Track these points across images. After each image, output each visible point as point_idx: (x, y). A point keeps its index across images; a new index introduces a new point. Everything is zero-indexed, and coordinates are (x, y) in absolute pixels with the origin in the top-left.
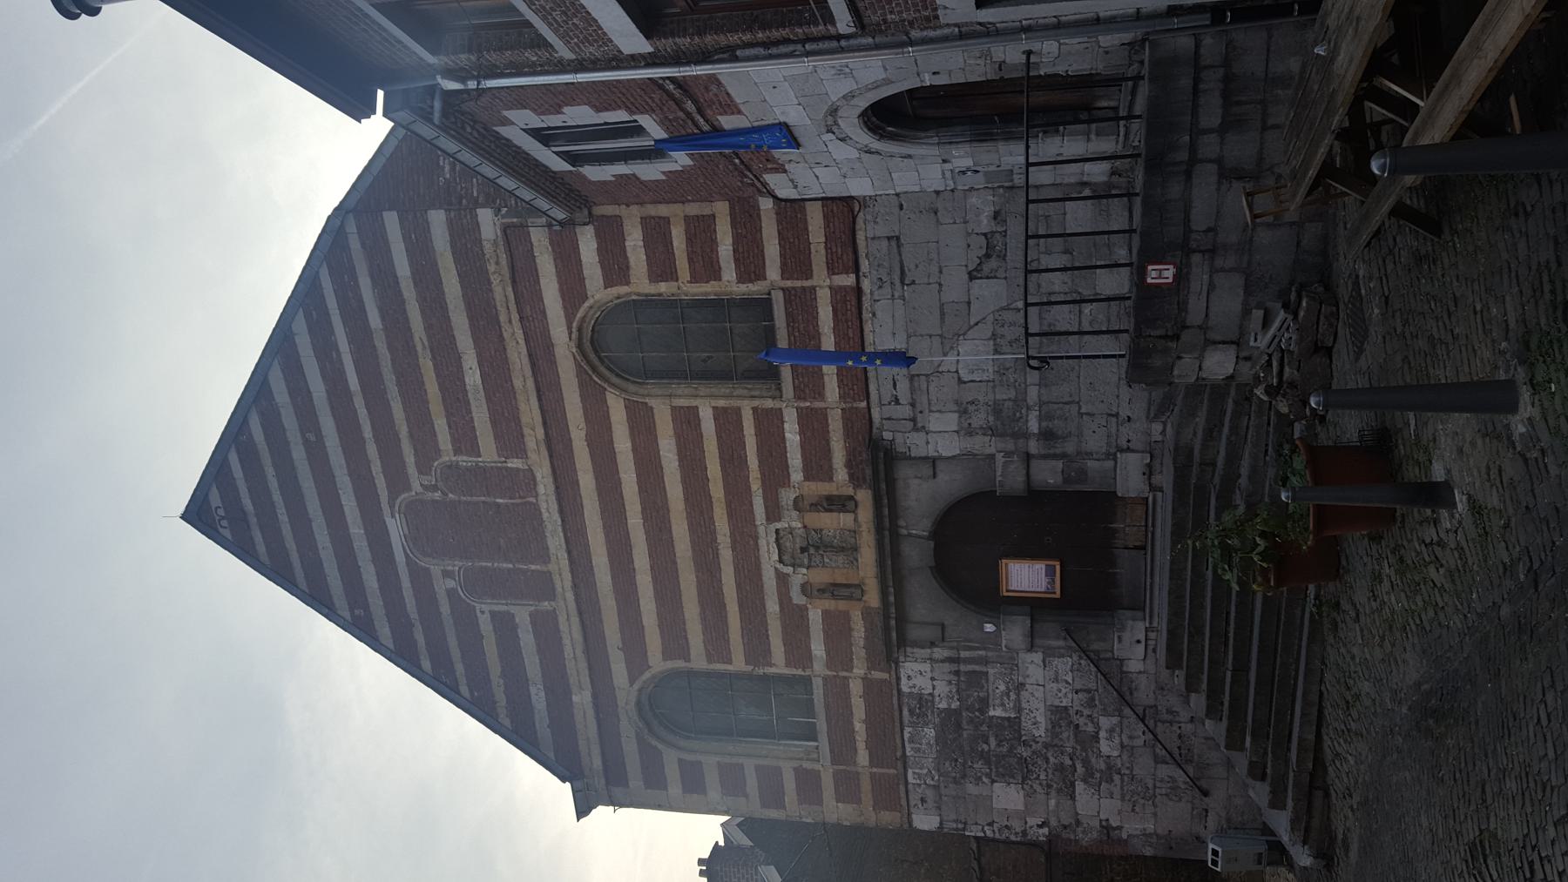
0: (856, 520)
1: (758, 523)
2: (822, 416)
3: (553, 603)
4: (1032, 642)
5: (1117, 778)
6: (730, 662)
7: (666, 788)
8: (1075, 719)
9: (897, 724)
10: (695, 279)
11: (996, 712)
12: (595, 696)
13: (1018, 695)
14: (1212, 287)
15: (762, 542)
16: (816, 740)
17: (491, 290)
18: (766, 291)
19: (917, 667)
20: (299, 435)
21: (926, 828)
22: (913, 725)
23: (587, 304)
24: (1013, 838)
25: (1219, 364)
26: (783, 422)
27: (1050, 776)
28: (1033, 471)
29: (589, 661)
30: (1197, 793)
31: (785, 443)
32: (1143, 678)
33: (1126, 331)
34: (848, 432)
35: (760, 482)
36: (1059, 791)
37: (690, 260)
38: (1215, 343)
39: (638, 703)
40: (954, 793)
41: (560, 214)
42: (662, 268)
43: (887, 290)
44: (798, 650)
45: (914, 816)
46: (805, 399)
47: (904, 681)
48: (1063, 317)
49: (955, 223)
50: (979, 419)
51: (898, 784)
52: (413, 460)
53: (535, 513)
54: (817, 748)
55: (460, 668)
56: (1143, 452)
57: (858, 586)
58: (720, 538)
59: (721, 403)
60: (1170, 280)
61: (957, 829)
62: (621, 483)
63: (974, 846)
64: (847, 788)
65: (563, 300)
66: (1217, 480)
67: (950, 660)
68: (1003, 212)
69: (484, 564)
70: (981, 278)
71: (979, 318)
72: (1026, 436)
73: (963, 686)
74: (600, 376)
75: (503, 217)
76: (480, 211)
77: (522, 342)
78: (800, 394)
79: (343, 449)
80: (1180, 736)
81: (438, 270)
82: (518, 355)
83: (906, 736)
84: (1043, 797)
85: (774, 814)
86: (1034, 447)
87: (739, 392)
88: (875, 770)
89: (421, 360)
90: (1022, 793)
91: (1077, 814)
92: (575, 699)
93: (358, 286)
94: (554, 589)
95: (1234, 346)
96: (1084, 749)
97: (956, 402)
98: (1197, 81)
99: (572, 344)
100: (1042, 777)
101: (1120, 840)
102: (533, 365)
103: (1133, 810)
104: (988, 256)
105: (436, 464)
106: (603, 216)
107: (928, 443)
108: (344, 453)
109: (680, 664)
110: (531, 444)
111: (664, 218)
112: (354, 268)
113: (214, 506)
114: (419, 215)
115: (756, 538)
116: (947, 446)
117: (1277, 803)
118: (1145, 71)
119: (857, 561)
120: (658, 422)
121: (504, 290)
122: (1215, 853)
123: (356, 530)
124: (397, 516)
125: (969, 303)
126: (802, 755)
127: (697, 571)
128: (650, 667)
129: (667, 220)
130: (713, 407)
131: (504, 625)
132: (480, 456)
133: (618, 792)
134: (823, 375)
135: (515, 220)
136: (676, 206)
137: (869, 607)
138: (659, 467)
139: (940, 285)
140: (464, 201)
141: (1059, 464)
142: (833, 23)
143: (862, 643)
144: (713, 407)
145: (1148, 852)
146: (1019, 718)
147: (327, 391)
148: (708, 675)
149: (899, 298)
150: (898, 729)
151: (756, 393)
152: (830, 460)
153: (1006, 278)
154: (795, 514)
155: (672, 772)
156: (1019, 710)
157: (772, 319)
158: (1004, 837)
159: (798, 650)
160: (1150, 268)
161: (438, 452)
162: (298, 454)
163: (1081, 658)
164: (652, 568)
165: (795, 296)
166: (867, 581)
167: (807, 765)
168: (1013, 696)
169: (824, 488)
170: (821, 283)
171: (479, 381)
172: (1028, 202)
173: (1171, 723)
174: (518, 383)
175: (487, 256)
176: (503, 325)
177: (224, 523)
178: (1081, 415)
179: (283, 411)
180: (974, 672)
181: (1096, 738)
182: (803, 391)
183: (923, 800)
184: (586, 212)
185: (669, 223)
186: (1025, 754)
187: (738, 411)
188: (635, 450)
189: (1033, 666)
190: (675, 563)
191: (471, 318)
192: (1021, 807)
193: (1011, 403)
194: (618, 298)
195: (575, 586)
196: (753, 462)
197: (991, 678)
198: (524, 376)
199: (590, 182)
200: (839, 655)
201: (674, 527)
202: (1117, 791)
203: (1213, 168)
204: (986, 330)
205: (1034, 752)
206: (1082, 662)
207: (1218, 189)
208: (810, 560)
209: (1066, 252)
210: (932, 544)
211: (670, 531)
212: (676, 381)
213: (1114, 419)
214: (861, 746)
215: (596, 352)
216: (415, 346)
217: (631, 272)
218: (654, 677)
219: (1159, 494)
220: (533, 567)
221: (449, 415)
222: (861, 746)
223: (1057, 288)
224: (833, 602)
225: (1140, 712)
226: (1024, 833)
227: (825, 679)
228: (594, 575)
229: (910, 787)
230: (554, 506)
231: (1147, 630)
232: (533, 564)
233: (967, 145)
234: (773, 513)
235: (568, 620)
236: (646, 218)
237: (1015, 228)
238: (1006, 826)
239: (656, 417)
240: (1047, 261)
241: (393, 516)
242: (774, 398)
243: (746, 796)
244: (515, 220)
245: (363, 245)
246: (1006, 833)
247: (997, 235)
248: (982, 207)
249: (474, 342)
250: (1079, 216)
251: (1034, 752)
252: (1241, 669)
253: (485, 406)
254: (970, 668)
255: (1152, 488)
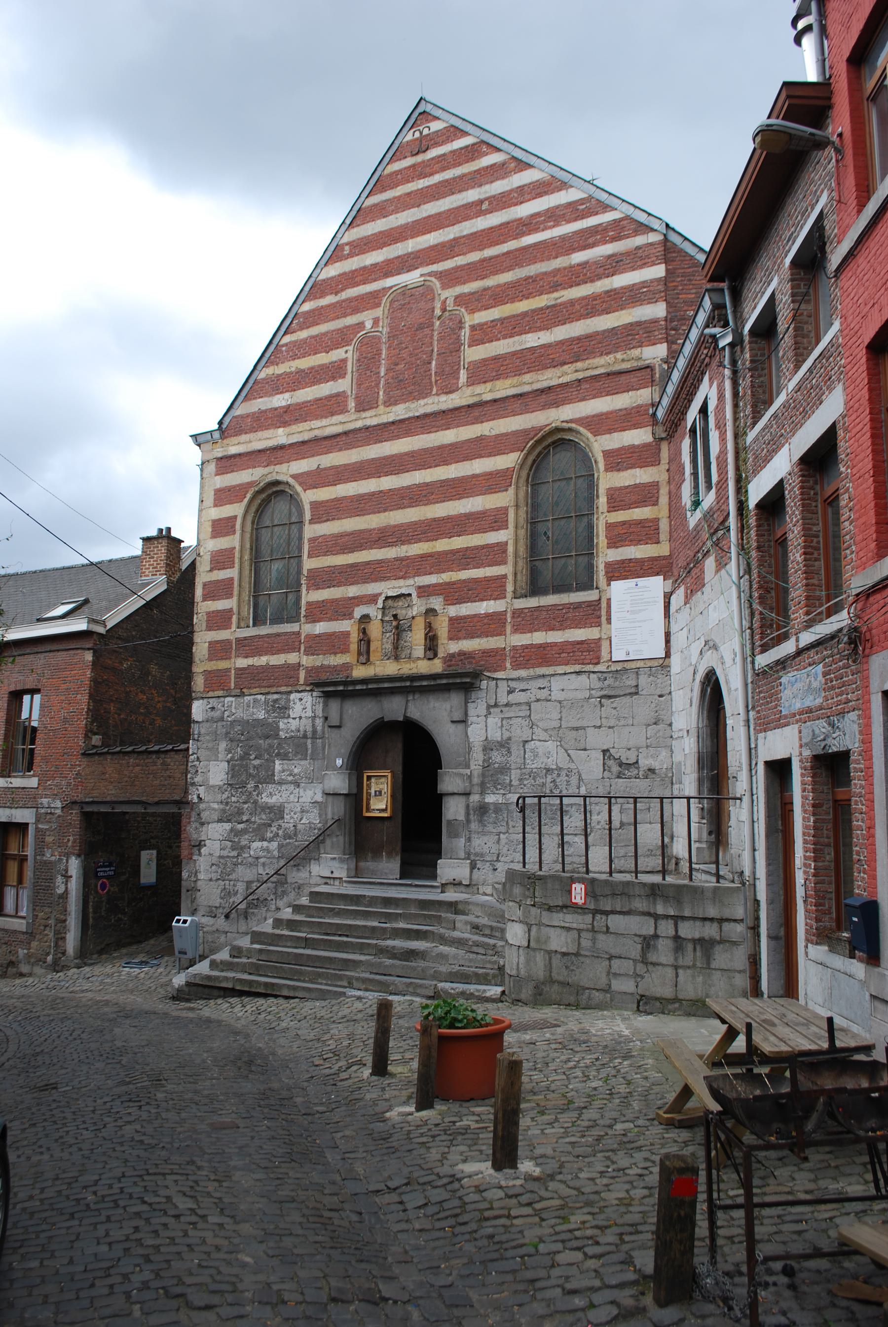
0: (419, 658)
1: (416, 579)
2: (501, 633)
3: (353, 410)
4: (329, 794)
5: (235, 853)
6: (310, 556)
7: (215, 505)
8: (275, 824)
9: (267, 690)
10: (609, 526)
11: (278, 765)
12: (282, 447)
13: (291, 783)
14: (568, 929)
15: (401, 582)
16: (254, 625)
17: (602, 355)
18: (600, 586)
19: (309, 705)
20: (487, 195)
21: (194, 711)
22: (266, 702)
23: (590, 435)
24: (189, 776)
25: (516, 933)
26: (495, 599)
27: (234, 805)
28: (456, 798)
29: (309, 441)
30: (227, 910)
31: (479, 601)
32: (307, 875)
33: (541, 869)
34: (488, 653)
35: (448, 580)
36: (224, 811)
37: (624, 523)
38: (529, 930)
39: (277, 483)
40: (218, 732)
41: (660, 413)
42: (618, 500)
43: (599, 685)
44: (319, 612)
45: (201, 701)
46: (513, 617)
47: (299, 695)
48: (574, 821)
49: (647, 738)
50: (497, 757)
51: (223, 690)
52: (466, 291)
53: (424, 393)
54: (248, 627)
55: (303, 334)
56: (471, 879)
57: (368, 660)
58: (404, 548)
59: (511, 549)
60: (574, 901)
61: (194, 734)
62: (447, 465)
63: (183, 747)
64: (219, 650)
65: (593, 416)
66: (442, 931)
67: (314, 731)
68: (654, 776)
69: (384, 352)
70: (604, 759)
71: (573, 757)
72: (482, 793)
73: (296, 741)
74: (533, 447)
75: (660, 365)
76: (664, 346)
77: (561, 381)
78: (517, 613)
79: (476, 233)
80: (266, 899)
81: (617, 311)
82: (549, 378)
83: (259, 697)
84: (219, 799)
85: (199, 592)
86: (475, 798)
87: (521, 563)
88: (233, 672)
89: (546, 296)
90: (221, 783)
91: (209, 823)
92: (281, 430)
93: (605, 243)
94: (364, 410)
95: (526, 945)
96: (254, 830)
97: (509, 739)
98: (712, 920)
99: (558, 424)
100: (233, 799)
101: (192, 854)
102: (542, 391)
103: (213, 864)
104: (621, 764)
105: (463, 310)
106: (660, 450)
107: (478, 716)
108: (472, 234)
109: (308, 516)
110: (479, 389)
111: (657, 501)
112: (620, 240)
113: (430, 125)
114: (663, 294)
115: (404, 577)
116: (476, 733)
117: (214, 965)
118: (725, 884)
119: (388, 659)
120: (495, 496)
121: (603, 366)
122: (185, 922)
123: (411, 245)
124: (422, 279)
125: (585, 750)
126: (242, 614)
127: (379, 529)
128: (305, 490)
129: (655, 503)
130: (507, 542)
131: (335, 371)
132: (469, 346)
133: (212, 468)
134: (531, 632)
135: (657, 375)
136: (667, 511)
137: (352, 670)
138: (459, 496)
139: (600, 727)
140: (673, 332)
141: (461, 817)
142: (762, 652)
143: (325, 663)
144: (507, 542)
145: (185, 875)
146: (274, 783)
147: (521, 219)
148: (300, 538)
149: (591, 694)
150: (264, 690)
151: (519, 577)
152: (465, 638)
153: (603, 778)
154: (423, 609)
155: (228, 511)
156: (281, 783)
157: (578, 590)
158: (189, 769)
159: (319, 612)
160: (583, 886)
161: (472, 312)
162: (472, 195)
163: (320, 829)
164: (381, 492)
165: (594, 610)
166: (372, 667)
167: (234, 619)
168: (290, 778)
169: (442, 629)
170: (604, 631)
171: (529, 345)
172: (662, 799)
173: (275, 894)
174: (527, 378)
175: (628, 352)
176: (574, 365)
177: (417, 135)
178: (499, 834)
179: (505, 181)
180: (307, 750)
181: (263, 839)
182: (519, 616)
183: (213, 708)
184: (664, 435)
185: (653, 505)
186: (249, 786)
187: (504, 562)
188: (474, 476)
189: (312, 794)
190: (385, 511)
191: (579, 339)
192: (212, 782)
193: (508, 781)
194: (596, 462)
195: (367, 428)
196: (464, 575)
197: (303, 762)
198: (532, 383)
199: (681, 442)
200: (317, 645)
201: (413, 510)
202: (225, 853)
203: (651, 932)
204: (563, 762)
205: (250, 793)
206: (316, 831)
207: (636, 935)
208: (388, 622)
209: (622, 824)
210: (401, 719)
211: (410, 507)
212: (529, 510)
213: (495, 859)
214: (250, 661)
215: (553, 443)
216: (557, 291)
217: (615, 474)
218: (298, 494)
219: (439, 890)
220: (381, 393)
221: (502, 320)
222: (250, 661)
223: (595, 817)
224: (356, 640)
225: (283, 871)
226: (193, 784)
227: (298, 633)
228: (376, 443)
229: (222, 699)
230: (429, 409)
231: (341, 878)
232: (384, 392)
233: (696, 750)
234: (425, 591)
235: (341, 423)
236: (657, 485)
237: (640, 787)
238: (197, 771)
239: (500, 494)
240: (615, 809)
241: (422, 275)
242: (514, 592)
243: (211, 570)
244: (657, 375)
245: (638, 248)
246: (192, 770)
247: (636, 772)
248: (658, 761)
249: (561, 341)
250: (649, 834)
251: (250, 793)
252: (308, 943)
253: (509, 350)
254: (310, 746)
255: (444, 887)
